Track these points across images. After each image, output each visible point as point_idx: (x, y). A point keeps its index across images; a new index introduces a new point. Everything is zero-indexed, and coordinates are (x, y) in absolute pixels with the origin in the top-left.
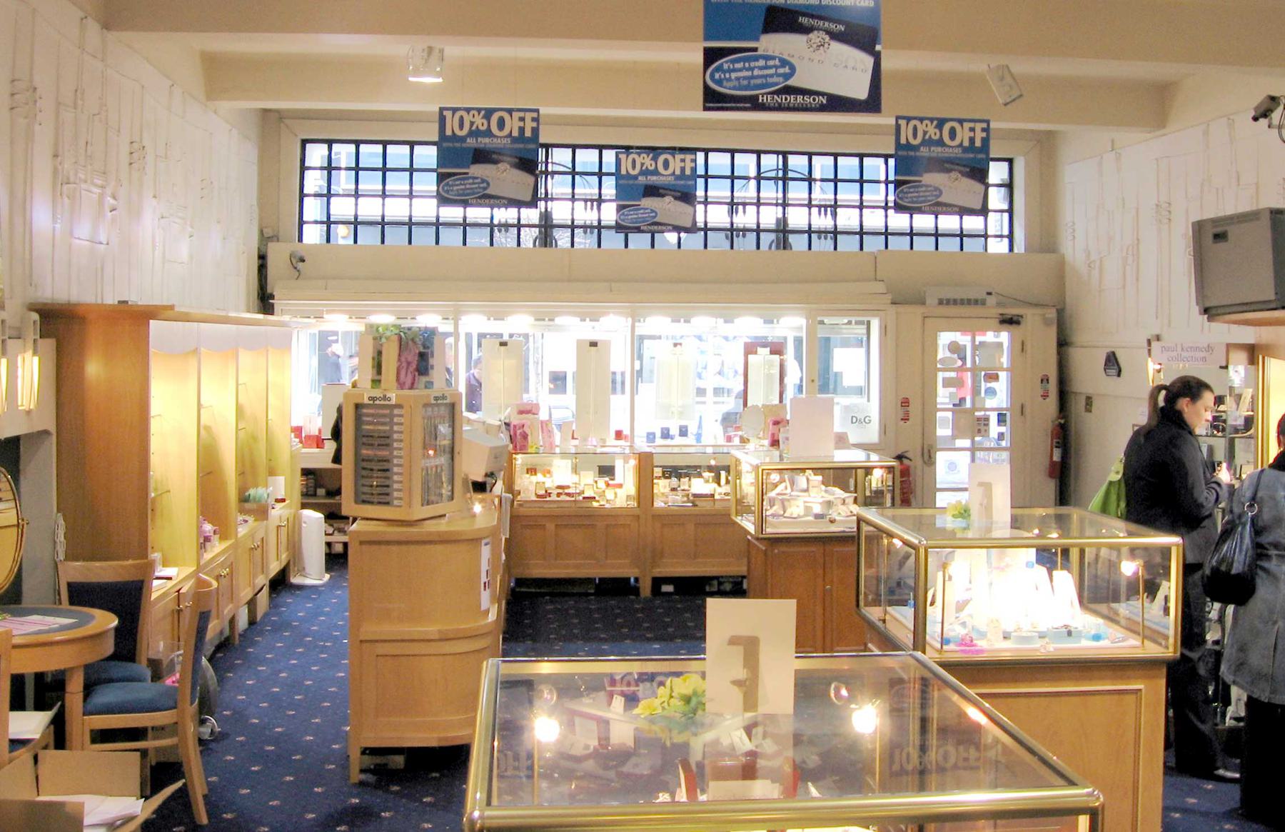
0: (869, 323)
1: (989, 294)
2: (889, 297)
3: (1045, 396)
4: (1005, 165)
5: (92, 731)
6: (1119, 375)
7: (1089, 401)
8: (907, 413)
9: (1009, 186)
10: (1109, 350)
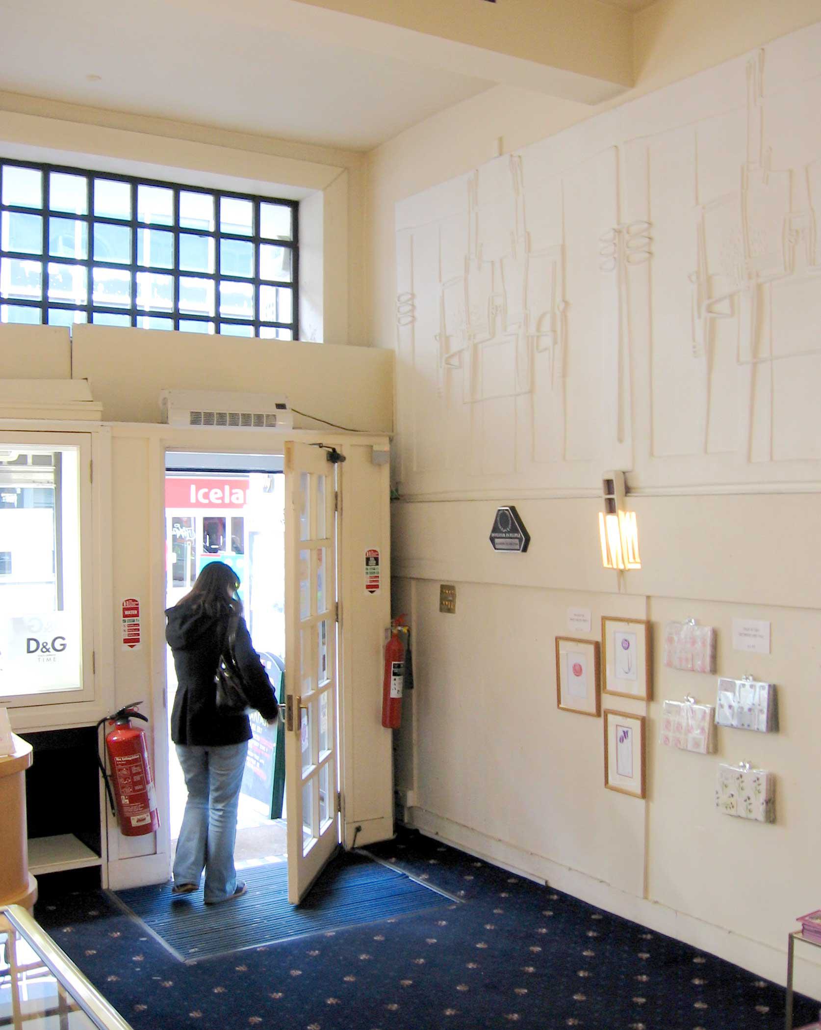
0: (59, 456)
1: (281, 406)
2: (98, 406)
3: (372, 587)
4: (287, 211)
5: (242, 518)
6: (525, 550)
7: (448, 597)
8: (135, 628)
9: (293, 245)
10: (502, 505)
